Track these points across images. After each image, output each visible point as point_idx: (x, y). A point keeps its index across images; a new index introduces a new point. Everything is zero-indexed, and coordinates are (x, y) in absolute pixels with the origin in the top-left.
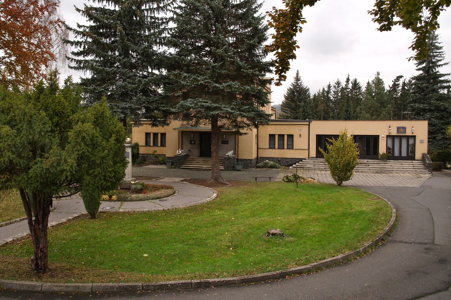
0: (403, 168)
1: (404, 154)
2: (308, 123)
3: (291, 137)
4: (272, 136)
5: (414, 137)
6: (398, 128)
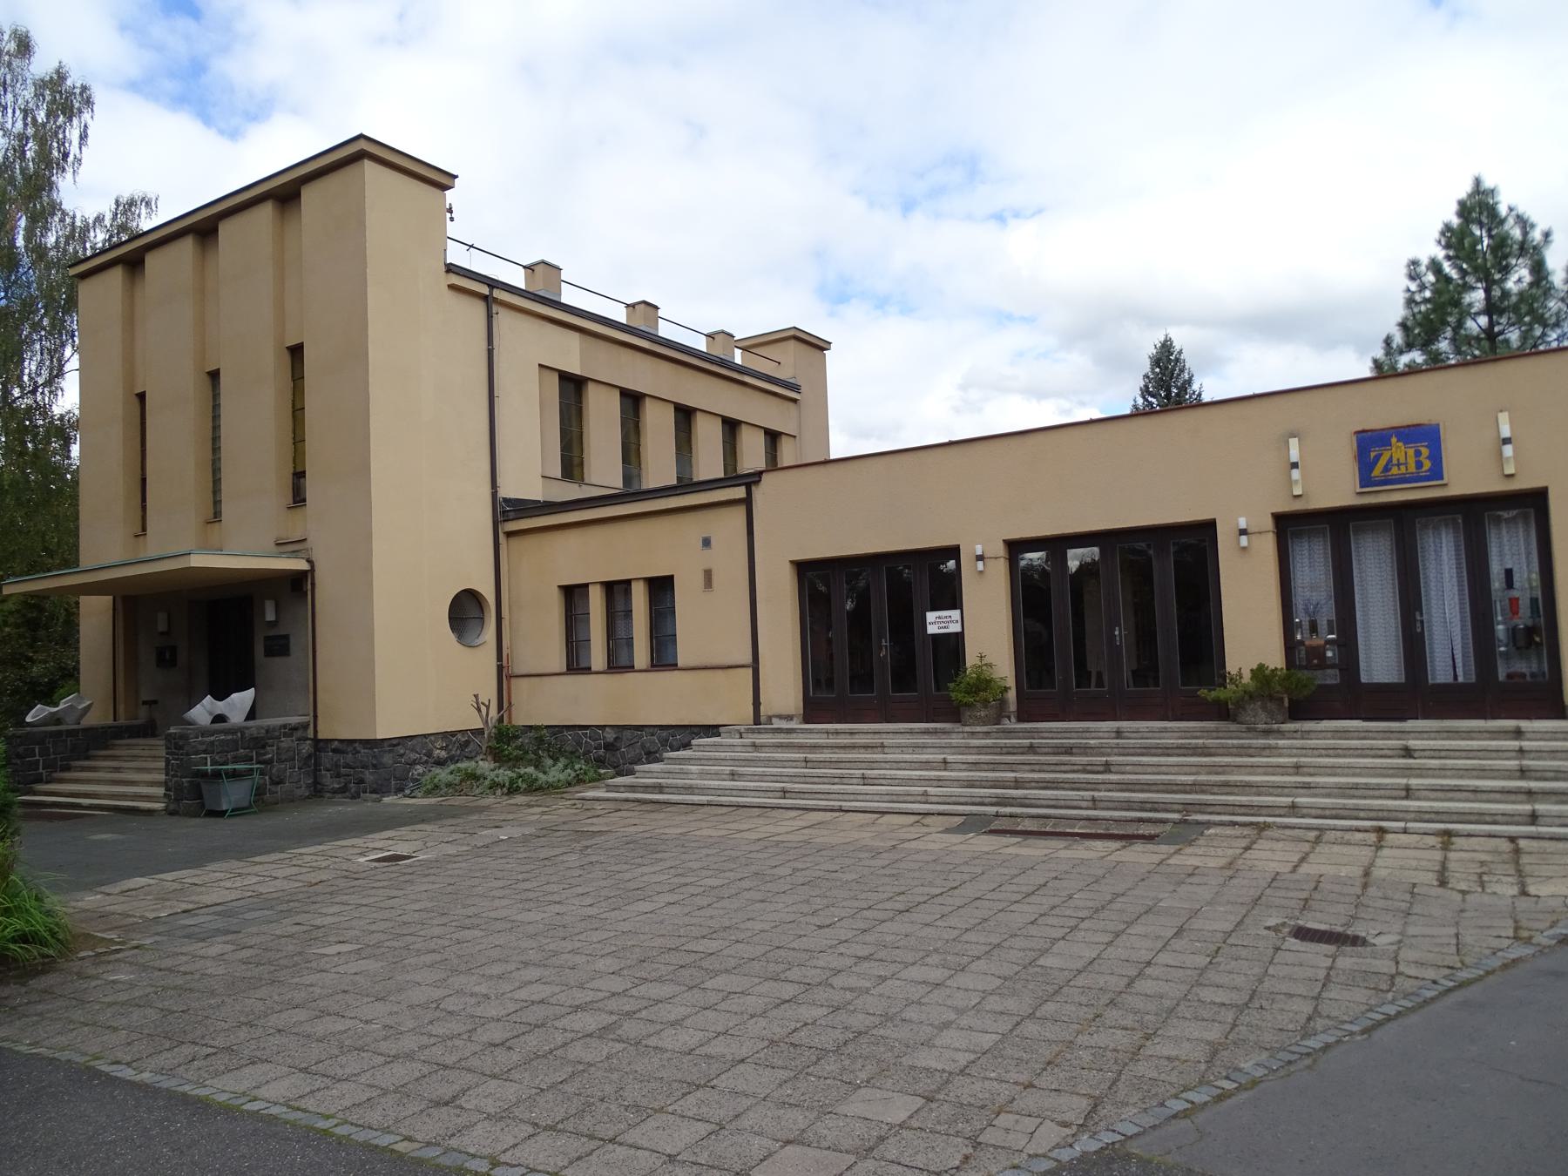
0: (1408, 792)
1: (1448, 657)
2: (740, 493)
3: (661, 587)
4: (573, 594)
5: (1533, 504)
6: (1369, 444)
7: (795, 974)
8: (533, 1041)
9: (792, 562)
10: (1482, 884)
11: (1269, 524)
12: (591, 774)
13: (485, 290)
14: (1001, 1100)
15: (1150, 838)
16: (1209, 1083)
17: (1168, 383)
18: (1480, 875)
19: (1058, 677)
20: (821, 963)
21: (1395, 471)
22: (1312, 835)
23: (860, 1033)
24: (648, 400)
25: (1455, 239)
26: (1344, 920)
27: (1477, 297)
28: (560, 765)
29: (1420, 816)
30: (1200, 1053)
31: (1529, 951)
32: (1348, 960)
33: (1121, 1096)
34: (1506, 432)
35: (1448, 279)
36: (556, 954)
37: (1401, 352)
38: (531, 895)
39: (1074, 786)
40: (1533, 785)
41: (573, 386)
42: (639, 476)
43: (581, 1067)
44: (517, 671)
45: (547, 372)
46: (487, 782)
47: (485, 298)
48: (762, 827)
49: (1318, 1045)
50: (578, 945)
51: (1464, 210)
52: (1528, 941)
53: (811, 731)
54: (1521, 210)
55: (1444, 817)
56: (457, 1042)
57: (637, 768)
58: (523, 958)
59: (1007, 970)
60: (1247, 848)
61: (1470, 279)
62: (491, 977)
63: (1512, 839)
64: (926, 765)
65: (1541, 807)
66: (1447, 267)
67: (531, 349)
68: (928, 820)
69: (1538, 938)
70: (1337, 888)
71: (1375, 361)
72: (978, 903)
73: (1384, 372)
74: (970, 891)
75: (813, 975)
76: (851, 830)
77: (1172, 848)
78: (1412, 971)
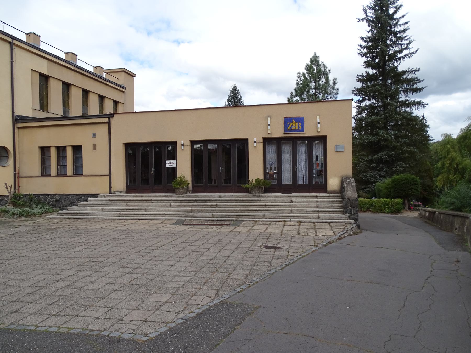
1: (302, 178)
2: (106, 120)
3: (77, 149)
4: (44, 150)
5: (323, 139)
6: (287, 121)
7: (129, 265)
8: (44, 291)
9: (123, 143)
10: (307, 233)
11: (262, 140)
12: (51, 210)
13: (10, 40)
14: (193, 293)
15: (228, 225)
16: (246, 284)
17: (235, 99)
18: (307, 231)
19: (204, 181)
20: (137, 262)
21: (293, 128)
22: (269, 223)
23: (151, 280)
24: (72, 86)
25: (309, 68)
26: (276, 243)
27: (313, 84)
28: (39, 207)
29: (294, 217)
30: (243, 277)
31: (317, 248)
32: (277, 253)
33: (224, 289)
34: (319, 121)
35: (307, 79)
36: (46, 265)
37: (294, 97)
38: (34, 248)
39: (208, 211)
40: (319, 209)
41: (44, 79)
42: (69, 112)
43: (62, 297)
44: (22, 176)
45: (34, 73)
46: (10, 213)
47: (10, 43)
48: (114, 225)
49: (271, 273)
50: (54, 262)
51: (312, 61)
52: (317, 246)
53: (128, 196)
54: (324, 63)
55: (299, 218)
56: (15, 294)
57: (68, 207)
58: (35, 267)
59: (192, 261)
60: (253, 227)
61: (312, 80)
62: (24, 274)
63: (314, 223)
64: (165, 206)
65: (320, 215)
66: (307, 75)
67: (26, 64)
68: (165, 222)
69: (319, 245)
70: (275, 236)
71: (288, 99)
72: (182, 244)
73: (290, 102)
74: (179, 240)
75: (134, 266)
76: (142, 225)
77: (234, 227)
78: (292, 254)
